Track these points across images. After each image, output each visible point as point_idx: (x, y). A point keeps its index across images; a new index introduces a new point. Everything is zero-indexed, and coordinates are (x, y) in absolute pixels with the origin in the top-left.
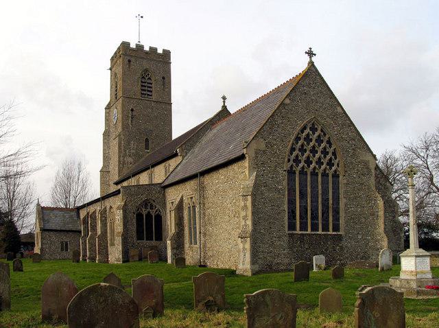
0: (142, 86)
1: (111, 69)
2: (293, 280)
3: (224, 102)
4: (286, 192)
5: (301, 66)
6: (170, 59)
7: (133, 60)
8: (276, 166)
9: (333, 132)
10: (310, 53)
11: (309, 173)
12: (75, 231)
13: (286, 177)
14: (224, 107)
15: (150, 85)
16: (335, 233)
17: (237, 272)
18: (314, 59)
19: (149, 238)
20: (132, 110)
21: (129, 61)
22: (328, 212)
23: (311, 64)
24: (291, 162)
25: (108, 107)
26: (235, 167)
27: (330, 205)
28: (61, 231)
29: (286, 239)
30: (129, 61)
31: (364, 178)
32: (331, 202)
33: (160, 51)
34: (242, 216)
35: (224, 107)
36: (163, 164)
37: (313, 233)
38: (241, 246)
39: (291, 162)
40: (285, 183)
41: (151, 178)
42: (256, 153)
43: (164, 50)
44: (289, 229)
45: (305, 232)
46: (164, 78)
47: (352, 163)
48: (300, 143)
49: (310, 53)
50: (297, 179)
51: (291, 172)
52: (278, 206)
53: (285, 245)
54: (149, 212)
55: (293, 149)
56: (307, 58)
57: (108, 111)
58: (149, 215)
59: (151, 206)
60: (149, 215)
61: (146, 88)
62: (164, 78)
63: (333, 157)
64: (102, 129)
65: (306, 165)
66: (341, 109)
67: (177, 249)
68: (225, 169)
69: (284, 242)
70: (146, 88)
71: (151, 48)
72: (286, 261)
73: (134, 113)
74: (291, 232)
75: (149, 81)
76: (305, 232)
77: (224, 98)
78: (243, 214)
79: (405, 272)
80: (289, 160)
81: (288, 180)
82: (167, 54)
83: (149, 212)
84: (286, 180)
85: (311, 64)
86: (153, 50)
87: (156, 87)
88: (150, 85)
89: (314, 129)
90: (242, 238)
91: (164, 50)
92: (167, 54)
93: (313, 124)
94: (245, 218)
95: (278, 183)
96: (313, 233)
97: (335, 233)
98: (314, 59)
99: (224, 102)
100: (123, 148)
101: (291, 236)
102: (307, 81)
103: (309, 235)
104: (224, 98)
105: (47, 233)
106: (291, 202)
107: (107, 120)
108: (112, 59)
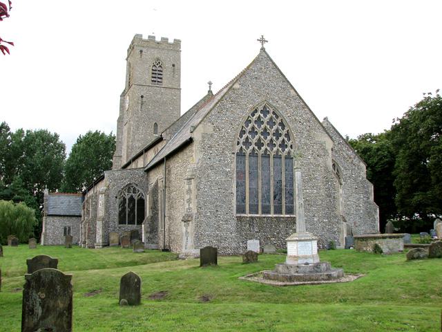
0: (161, 78)
1: (127, 60)
2: (199, 265)
3: (210, 87)
4: (235, 175)
5: (254, 52)
6: (180, 48)
7: (144, 50)
8: (223, 149)
9: (286, 114)
10: (262, 40)
11: (247, 155)
12: (77, 216)
13: (235, 160)
14: (210, 92)
15: (161, 73)
16: (288, 216)
17: (180, 256)
18: (266, 45)
19: (131, 222)
20: (142, 97)
21: (141, 51)
22: (281, 194)
23: (263, 49)
24: (241, 145)
25: (123, 95)
26: (187, 151)
27: (284, 188)
28: (64, 216)
29: (234, 222)
30: (141, 51)
31: (321, 160)
32: (284, 183)
33: (171, 41)
34: (186, 199)
35: (210, 92)
36: (153, 148)
37: (264, 215)
38: (184, 229)
39: (241, 145)
40: (234, 165)
41: (137, 166)
42: (203, 137)
43: (175, 40)
44: (238, 211)
45: (256, 215)
46: (174, 65)
47: (306, 144)
48: (250, 125)
49: (262, 40)
50: (247, 162)
51: (241, 155)
52: (225, 189)
53: (233, 229)
54: (132, 196)
55: (243, 132)
56: (259, 46)
57: (123, 98)
58: (132, 199)
59: (134, 189)
60: (132, 199)
61: (157, 76)
62: (174, 65)
63: (286, 139)
64: (117, 115)
65: (256, 148)
66: (294, 93)
67: (151, 232)
68: (182, 153)
69: (232, 225)
70: (157, 76)
71: (162, 38)
72: (234, 245)
73: (144, 99)
74: (239, 215)
75: (160, 69)
76: (256, 215)
77: (210, 83)
78: (187, 197)
79: (291, 256)
80: (238, 143)
81: (237, 162)
82: (177, 43)
83: (132, 196)
84: (235, 163)
85: (263, 49)
86: (165, 40)
87: (166, 74)
88: (161, 73)
89: (265, 112)
90: (185, 222)
91: (175, 40)
92: (177, 43)
93: (265, 107)
94: (189, 201)
95: (226, 165)
96: (264, 215)
97: (288, 216)
98: (266, 45)
99: (210, 87)
100: (131, 133)
101: (239, 219)
102: (259, 66)
103: (259, 218)
104: (210, 83)
105: (51, 218)
106: (240, 185)
107: (122, 107)
108: (128, 50)
